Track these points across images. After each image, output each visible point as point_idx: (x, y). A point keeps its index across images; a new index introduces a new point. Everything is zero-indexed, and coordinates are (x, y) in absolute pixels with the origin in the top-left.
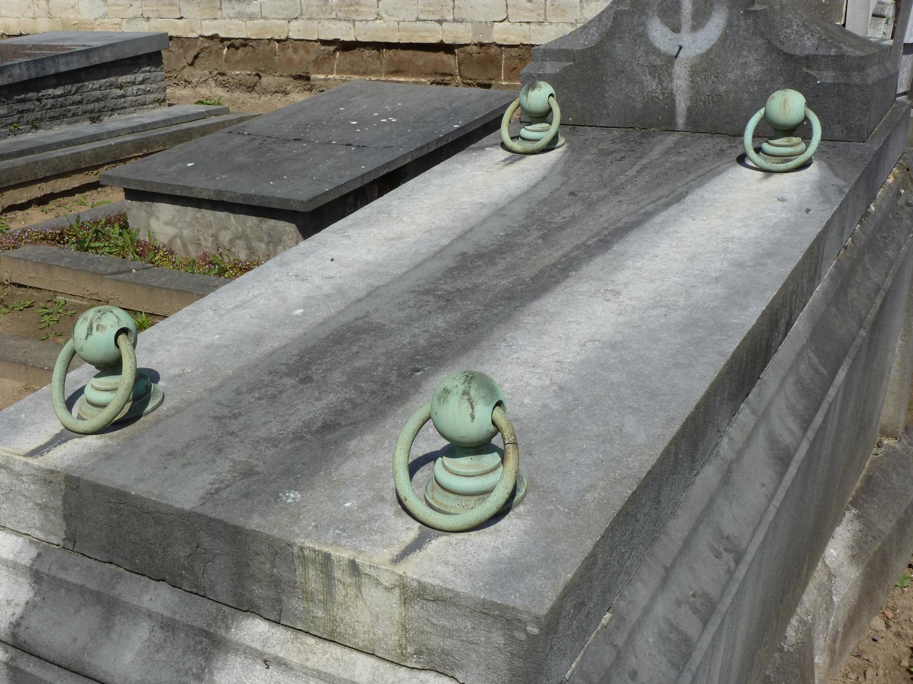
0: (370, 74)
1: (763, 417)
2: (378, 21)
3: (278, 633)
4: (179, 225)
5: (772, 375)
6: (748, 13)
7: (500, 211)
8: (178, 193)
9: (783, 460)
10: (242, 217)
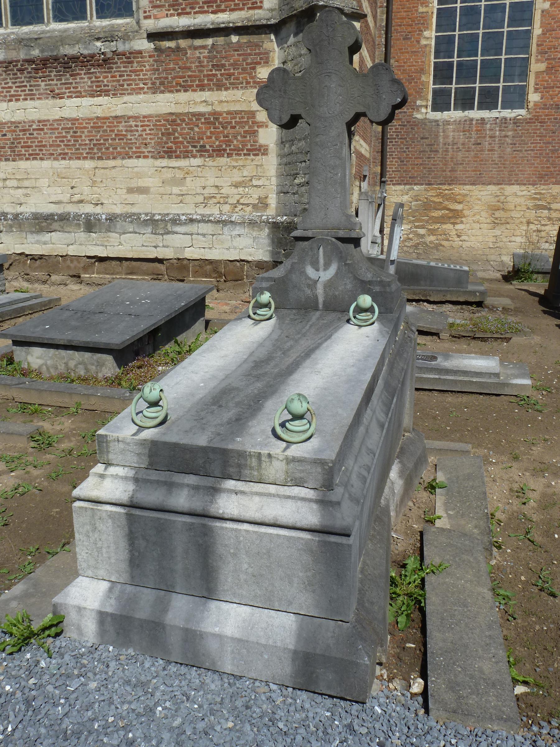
0: (116, 274)
1: (374, 412)
2: (120, 246)
3: (239, 483)
4: (45, 358)
5: (375, 398)
6: (346, 264)
7: (261, 345)
8: (46, 342)
9: (382, 426)
10: (82, 353)
